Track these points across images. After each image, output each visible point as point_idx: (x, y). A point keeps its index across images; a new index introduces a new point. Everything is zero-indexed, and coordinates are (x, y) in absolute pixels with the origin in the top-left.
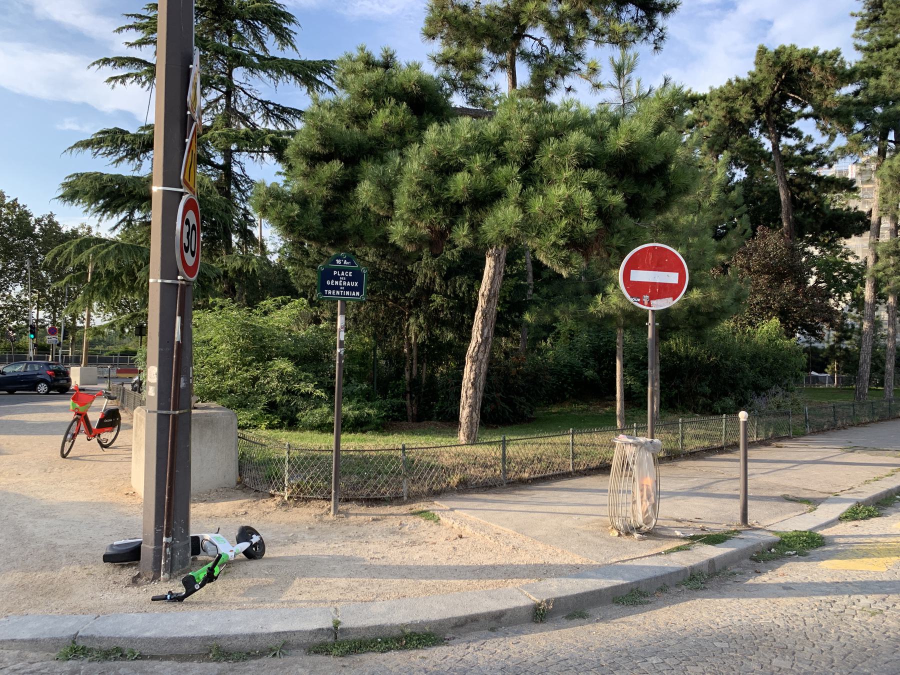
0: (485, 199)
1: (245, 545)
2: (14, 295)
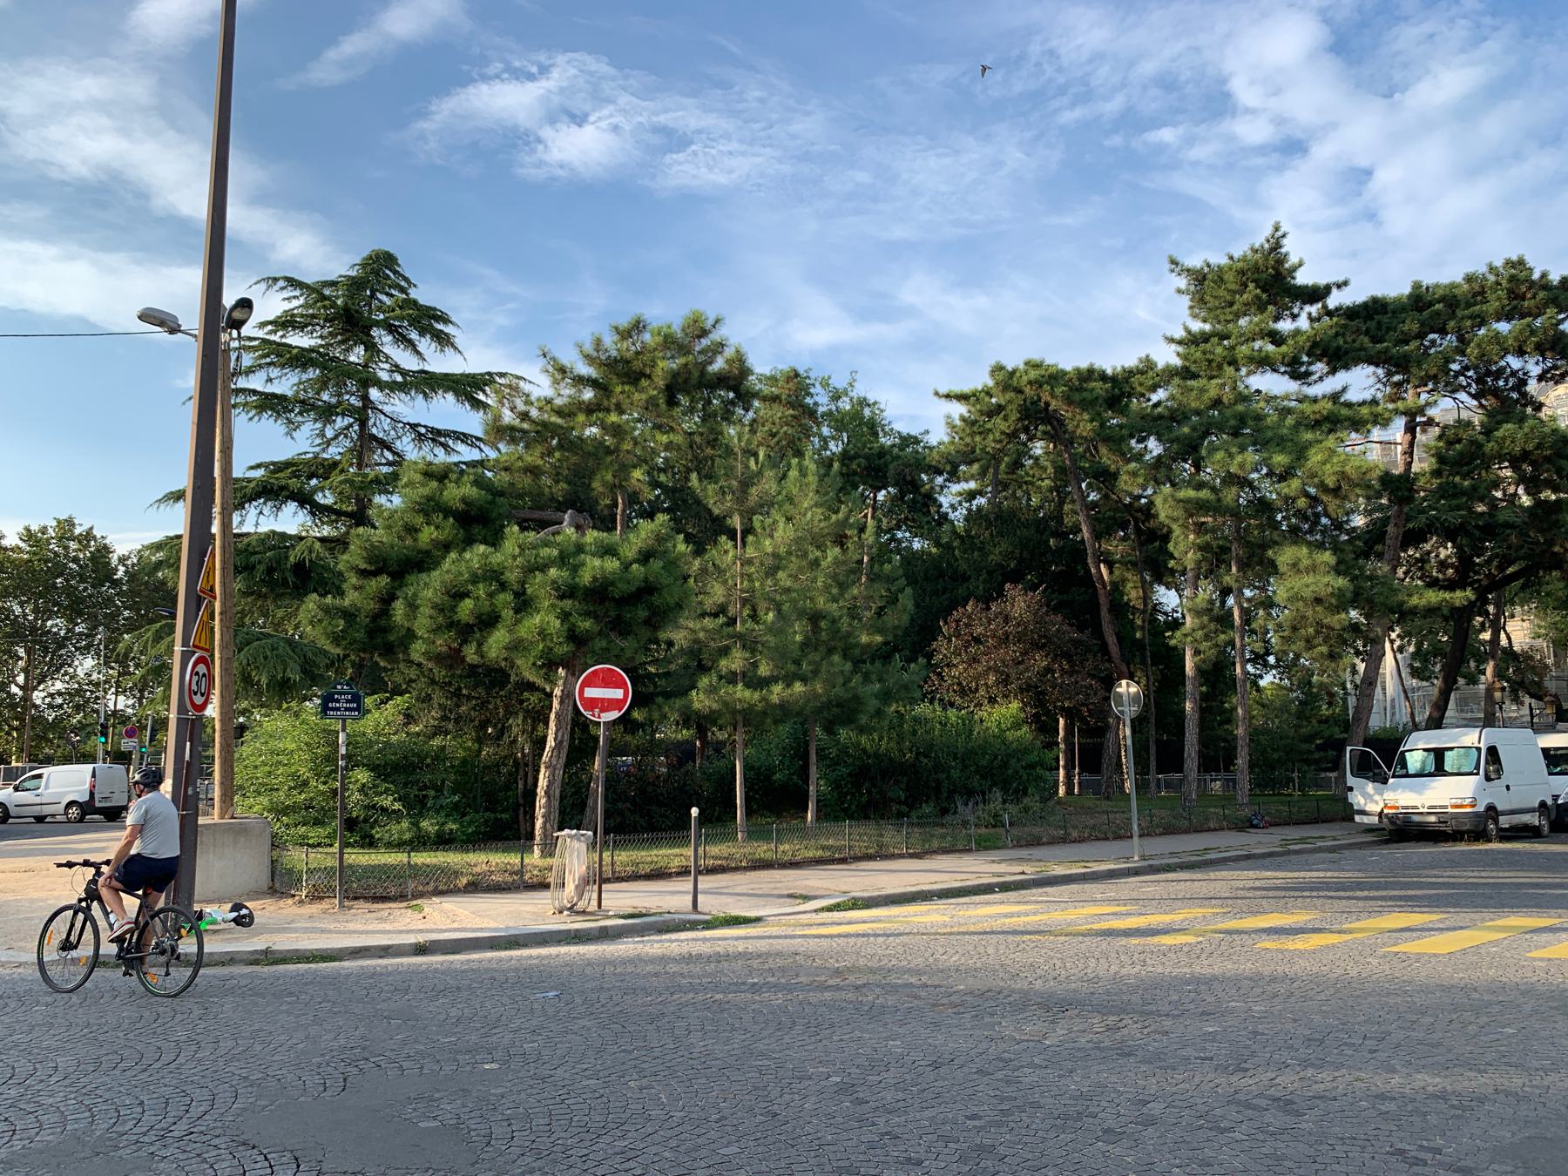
0: (488, 621)
1: (235, 914)
2: (81, 673)
